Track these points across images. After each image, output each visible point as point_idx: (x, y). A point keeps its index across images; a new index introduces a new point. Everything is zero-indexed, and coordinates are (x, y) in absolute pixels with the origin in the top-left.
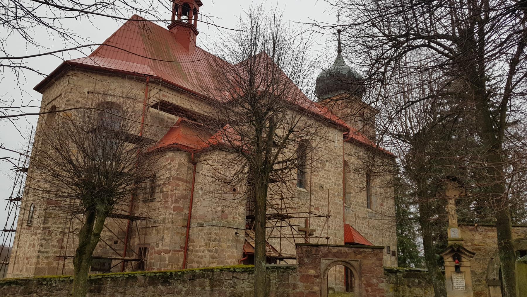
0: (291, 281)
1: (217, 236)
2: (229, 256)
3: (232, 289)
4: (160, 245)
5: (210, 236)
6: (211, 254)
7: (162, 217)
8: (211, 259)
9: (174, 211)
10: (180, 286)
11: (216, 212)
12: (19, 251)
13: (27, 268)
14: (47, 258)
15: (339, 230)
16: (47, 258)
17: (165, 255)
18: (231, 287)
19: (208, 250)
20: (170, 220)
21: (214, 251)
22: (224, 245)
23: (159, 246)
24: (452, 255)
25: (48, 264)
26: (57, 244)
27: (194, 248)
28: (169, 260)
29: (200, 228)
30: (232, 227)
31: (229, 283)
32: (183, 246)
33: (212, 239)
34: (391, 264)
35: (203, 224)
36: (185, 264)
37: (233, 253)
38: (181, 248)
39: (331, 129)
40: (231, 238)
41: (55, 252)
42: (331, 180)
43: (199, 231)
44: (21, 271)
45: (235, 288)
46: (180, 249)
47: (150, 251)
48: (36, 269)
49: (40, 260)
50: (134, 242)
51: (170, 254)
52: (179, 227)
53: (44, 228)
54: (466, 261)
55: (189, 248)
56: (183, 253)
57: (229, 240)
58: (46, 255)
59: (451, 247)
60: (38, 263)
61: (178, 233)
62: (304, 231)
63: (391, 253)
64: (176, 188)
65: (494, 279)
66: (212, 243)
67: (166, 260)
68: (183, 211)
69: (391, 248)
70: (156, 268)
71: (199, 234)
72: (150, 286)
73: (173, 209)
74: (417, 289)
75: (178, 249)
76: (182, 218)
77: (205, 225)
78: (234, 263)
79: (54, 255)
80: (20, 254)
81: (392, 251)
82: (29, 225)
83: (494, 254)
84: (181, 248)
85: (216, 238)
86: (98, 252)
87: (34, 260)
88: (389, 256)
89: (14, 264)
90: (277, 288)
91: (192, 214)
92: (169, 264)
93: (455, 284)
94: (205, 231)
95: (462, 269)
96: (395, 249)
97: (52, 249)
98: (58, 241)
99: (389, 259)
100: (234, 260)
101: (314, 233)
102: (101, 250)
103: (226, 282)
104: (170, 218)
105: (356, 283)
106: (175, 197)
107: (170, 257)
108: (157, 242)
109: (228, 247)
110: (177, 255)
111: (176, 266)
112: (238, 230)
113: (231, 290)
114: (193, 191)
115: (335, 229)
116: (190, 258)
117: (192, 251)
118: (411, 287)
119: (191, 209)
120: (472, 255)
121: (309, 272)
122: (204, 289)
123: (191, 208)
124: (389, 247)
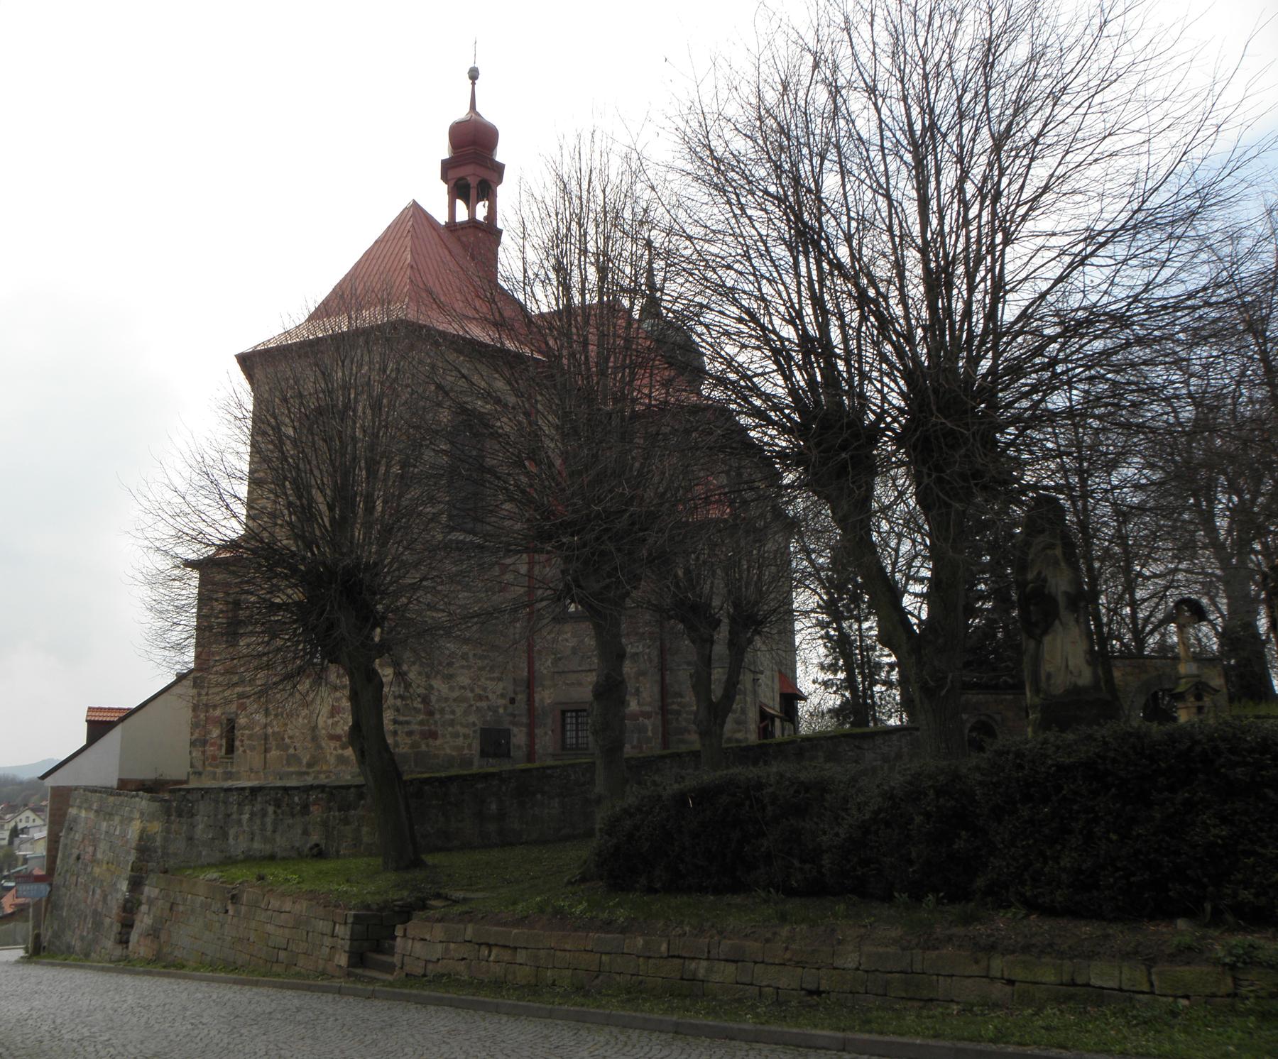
14: (410, 734)
16: (410, 734)
25: (413, 746)
49: (399, 739)
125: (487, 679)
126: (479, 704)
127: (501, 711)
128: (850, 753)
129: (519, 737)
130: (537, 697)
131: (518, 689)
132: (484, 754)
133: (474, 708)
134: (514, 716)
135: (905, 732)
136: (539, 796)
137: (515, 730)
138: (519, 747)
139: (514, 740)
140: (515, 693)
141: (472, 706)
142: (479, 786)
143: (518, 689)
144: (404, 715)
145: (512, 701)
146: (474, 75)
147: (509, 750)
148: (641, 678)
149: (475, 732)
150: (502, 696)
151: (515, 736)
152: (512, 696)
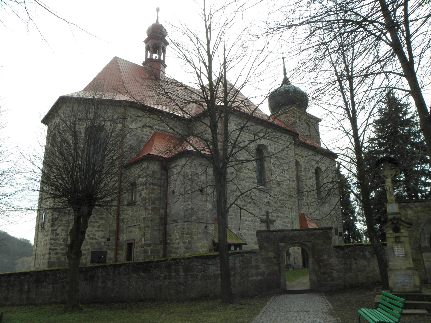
0: (253, 263)
1: (189, 230)
2: (200, 246)
3: (203, 273)
4: (143, 240)
5: (183, 230)
6: (185, 245)
7: (142, 217)
8: (185, 250)
9: (152, 211)
10: (158, 273)
11: (187, 210)
12: (37, 250)
13: (43, 262)
14: (57, 254)
15: (295, 219)
16: (57, 254)
17: (147, 248)
18: (201, 272)
19: (182, 242)
20: (149, 219)
21: (187, 242)
22: (195, 237)
23: (142, 241)
25: (58, 258)
27: (171, 241)
28: (151, 252)
29: (175, 224)
30: (201, 221)
31: (199, 268)
32: (162, 240)
33: (185, 232)
34: (339, 243)
35: (177, 221)
36: (165, 255)
38: (160, 241)
39: (284, 135)
40: (201, 231)
41: (62, 249)
42: (286, 177)
43: (174, 227)
44: (40, 265)
45: (205, 272)
46: (160, 243)
47: (136, 245)
48: (48, 263)
49: (51, 256)
50: (123, 239)
51: (152, 247)
52: (157, 224)
53: (52, 230)
54: (404, 232)
55: (167, 241)
57: (200, 233)
58: (55, 252)
59: (391, 220)
60: (50, 258)
61: (157, 229)
62: (265, 222)
63: (339, 234)
64: (152, 192)
65: (426, 246)
66: (185, 236)
67: (148, 252)
68: (159, 211)
69: (338, 230)
70: (141, 259)
71: (174, 229)
73: (151, 209)
74: (361, 261)
75: (158, 243)
76: (159, 217)
77: (178, 222)
78: (205, 251)
79: (61, 251)
80: (39, 252)
81: (339, 232)
82: (43, 228)
83: (424, 226)
84: (160, 241)
85: (188, 232)
86: (95, 248)
87: (47, 256)
88: (337, 237)
89: (35, 259)
90: (242, 270)
91: (168, 213)
92: (151, 256)
93: (396, 253)
94: (179, 227)
96: (342, 231)
97: (59, 247)
98: (64, 241)
99: (337, 239)
100: (206, 249)
101: (275, 222)
102: (97, 246)
103: (197, 267)
104: (149, 217)
105: (311, 260)
106: (152, 199)
108: (140, 237)
109: (199, 239)
110: (157, 248)
111: (157, 257)
112: (208, 224)
113: (202, 274)
114: (167, 193)
115: (292, 218)
116: (168, 249)
117: (169, 244)
118: (356, 260)
119: (167, 209)
120: (410, 226)
121: (269, 255)
122: (178, 274)
123: (166, 208)
124: (336, 230)
125: (96, 231)
126: (91, 241)
127: (103, 244)
128: (199, 267)
129: (111, 255)
130: (121, 238)
131: (111, 235)
132: (92, 261)
133: (89, 243)
134: (109, 246)
135: (239, 255)
136: (44, 283)
137: (109, 252)
138: (111, 259)
139: (108, 256)
140: (110, 236)
141: (88, 242)
142: (22, 278)
143: (111, 235)
144: (54, 246)
145: (108, 240)
146: (158, 10)
147: (105, 260)
148: (146, 228)
149: (89, 253)
150: (104, 238)
151: (109, 254)
152: (108, 237)
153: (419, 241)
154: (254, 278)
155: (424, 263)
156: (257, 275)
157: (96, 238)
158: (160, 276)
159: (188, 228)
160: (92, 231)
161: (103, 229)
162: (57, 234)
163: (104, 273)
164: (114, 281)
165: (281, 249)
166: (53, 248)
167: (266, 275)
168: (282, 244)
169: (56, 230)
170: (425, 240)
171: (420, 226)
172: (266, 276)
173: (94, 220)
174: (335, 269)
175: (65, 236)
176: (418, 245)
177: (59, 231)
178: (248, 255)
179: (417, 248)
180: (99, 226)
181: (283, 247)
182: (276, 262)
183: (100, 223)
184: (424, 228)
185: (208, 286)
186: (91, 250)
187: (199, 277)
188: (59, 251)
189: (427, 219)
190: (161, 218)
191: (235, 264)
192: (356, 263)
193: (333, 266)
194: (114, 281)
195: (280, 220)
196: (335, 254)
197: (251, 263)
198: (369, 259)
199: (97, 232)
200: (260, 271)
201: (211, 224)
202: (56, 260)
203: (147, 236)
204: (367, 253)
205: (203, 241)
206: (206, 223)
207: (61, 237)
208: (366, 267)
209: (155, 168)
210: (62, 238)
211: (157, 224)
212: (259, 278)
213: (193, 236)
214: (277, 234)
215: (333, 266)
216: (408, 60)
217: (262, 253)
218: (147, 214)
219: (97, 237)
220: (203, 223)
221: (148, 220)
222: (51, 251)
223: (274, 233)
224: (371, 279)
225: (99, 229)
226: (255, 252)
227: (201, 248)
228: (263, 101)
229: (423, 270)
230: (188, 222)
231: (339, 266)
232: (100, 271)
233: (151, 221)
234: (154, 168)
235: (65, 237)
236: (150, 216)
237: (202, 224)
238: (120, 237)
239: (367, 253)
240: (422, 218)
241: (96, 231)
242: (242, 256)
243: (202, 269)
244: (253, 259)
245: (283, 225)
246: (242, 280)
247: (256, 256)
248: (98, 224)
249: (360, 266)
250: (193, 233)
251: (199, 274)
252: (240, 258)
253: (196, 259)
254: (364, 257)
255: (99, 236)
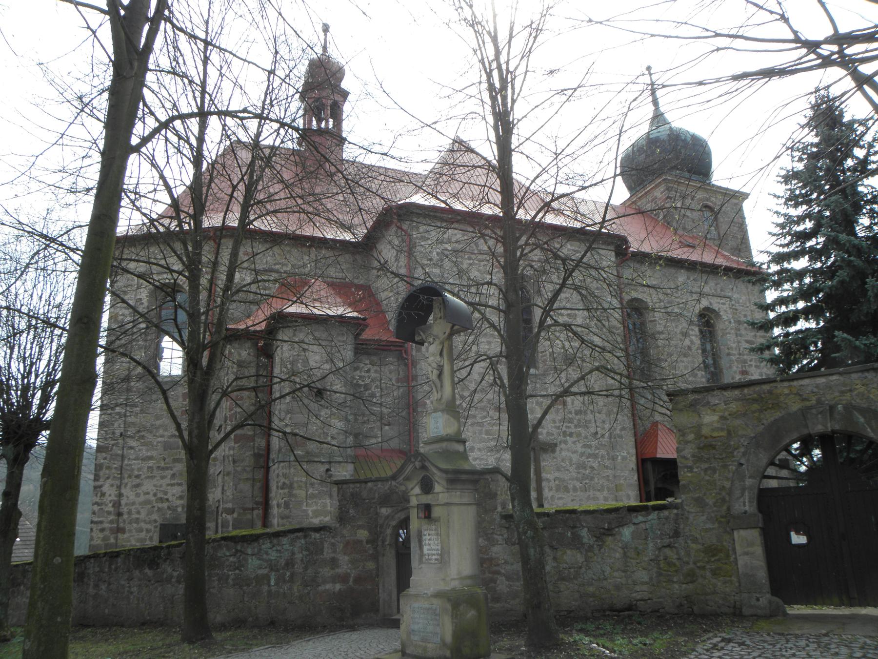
0: (327, 554)
2: (314, 512)
9: (235, 443)
14: (102, 530)
16: (102, 530)
18: (235, 570)
20: (231, 458)
24: (449, 476)
25: (105, 539)
26: (112, 509)
30: (316, 459)
31: (231, 562)
37: (325, 505)
38: (257, 503)
41: (111, 522)
45: (241, 570)
49: (94, 534)
51: (235, 515)
52: (248, 469)
53: (95, 487)
56: (261, 512)
58: (100, 527)
60: (92, 539)
61: (247, 479)
65: (745, 512)
67: (229, 525)
72: (135, 569)
74: (568, 552)
75: (250, 505)
79: (110, 526)
83: (744, 454)
85: (284, 483)
90: (306, 569)
95: (436, 512)
97: (107, 517)
98: (113, 506)
106: (236, 418)
107: (235, 520)
113: (235, 574)
118: (556, 549)
121: (358, 535)
125: (168, 485)
126: (160, 505)
127: (180, 509)
128: (231, 559)
133: (156, 509)
135: (301, 534)
141: (154, 507)
144: (98, 517)
149: (155, 527)
153: (727, 498)
154: (328, 586)
155: (736, 558)
156: (335, 579)
157: (167, 500)
158: (172, 577)
159: (284, 475)
160: (161, 486)
161: (179, 482)
162: (103, 495)
163: (97, 569)
164: (109, 584)
165: (381, 521)
166: (96, 519)
167: (351, 580)
168: (385, 511)
169: (101, 487)
170: (743, 495)
171: (733, 457)
172: (351, 583)
173: (165, 464)
174: (503, 571)
175: (116, 496)
176: (725, 508)
177: (105, 489)
178: (318, 535)
179: (722, 517)
180: (173, 476)
181: (387, 517)
182: (371, 552)
183: (175, 470)
184: (743, 461)
185: (246, 599)
186: (160, 521)
187: (231, 582)
188: (106, 525)
189: (752, 435)
190: (257, 456)
191: (293, 554)
192: (555, 559)
193: (498, 565)
194: (109, 584)
195: (574, 443)
196: (502, 535)
197: (322, 553)
198: (590, 548)
199: (169, 487)
200: (339, 571)
201: (342, 464)
202: (101, 543)
203: (228, 494)
204: (584, 533)
205: (320, 502)
206: (330, 462)
207: (110, 498)
208: (581, 568)
209: (243, 355)
210: (111, 501)
211: (248, 469)
212: (338, 587)
213: (294, 492)
214: (375, 488)
215: (498, 565)
216: (314, 119)
217: (345, 532)
218: (227, 449)
219: (169, 496)
220: (320, 462)
221: (229, 461)
222: (94, 526)
223: (369, 484)
224: (591, 599)
225: (173, 482)
226: (330, 529)
227: (316, 517)
228: (619, 144)
229: (734, 579)
230: (284, 462)
231: (512, 564)
232: (92, 565)
233: (234, 462)
234: (240, 354)
235: (115, 499)
236: (232, 452)
237: (319, 465)
238: (209, 495)
239: (584, 533)
240: (740, 433)
241: (168, 485)
242: (305, 537)
243: (235, 563)
244: (326, 545)
245: (582, 454)
246: (306, 591)
247: (333, 537)
248: (172, 472)
249: (565, 565)
250: (295, 485)
251: (230, 573)
252: (303, 541)
253: (225, 543)
254: (576, 543)
255: (173, 495)
